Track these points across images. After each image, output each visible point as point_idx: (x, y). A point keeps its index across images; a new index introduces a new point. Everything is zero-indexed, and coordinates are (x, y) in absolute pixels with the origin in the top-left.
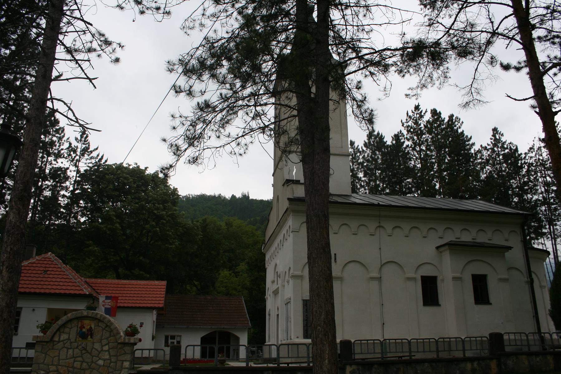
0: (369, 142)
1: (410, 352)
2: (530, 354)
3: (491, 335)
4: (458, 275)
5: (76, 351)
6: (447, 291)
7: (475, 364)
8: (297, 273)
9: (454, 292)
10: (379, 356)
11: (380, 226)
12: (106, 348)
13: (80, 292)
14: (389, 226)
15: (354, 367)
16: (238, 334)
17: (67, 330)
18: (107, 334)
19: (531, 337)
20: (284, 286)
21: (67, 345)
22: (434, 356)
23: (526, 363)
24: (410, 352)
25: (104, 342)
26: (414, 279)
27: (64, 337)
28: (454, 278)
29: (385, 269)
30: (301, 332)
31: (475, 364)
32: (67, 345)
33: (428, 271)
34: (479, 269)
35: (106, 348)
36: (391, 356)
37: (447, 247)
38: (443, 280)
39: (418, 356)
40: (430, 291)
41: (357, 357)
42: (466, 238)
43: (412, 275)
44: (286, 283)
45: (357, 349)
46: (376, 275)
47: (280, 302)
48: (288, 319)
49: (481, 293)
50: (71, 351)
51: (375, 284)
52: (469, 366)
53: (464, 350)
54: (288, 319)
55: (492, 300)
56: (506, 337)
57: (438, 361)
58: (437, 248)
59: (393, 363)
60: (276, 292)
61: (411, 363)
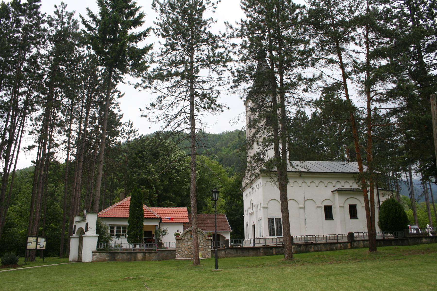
0: (297, 117)
1: (316, 240)
2: (364, 241)
3: (349, 233)
4: (342, 205)
5: (191, 243)
6: (336, 212)
7: (341, 245)
8: (265, 206)
9: (341, 213)
10: (304, 242)
11: (304, 182)
12: (202, 241)
13: (155, 217)
14: (308, 181)
15: (294, 246)
16: (225, 236)
17: (187, 235)
18: (202, 236)
19: (365, 234)
20: (257, 211)
21: (188, 240)
22: (325, 242)
23: (362, 244)
24: (316, 240)
25: (201, 239)
26: (321, 207)
27: (186, 238)
28: (340, 207)
29: (307, 202)
30: (268, 233)
31: (341, 245)
32: (188, 240)
33: (328, 203)
34: (352, 202)
35: (202, 241)
36: (309, 242)
37: (336, 192)
38: (335, 208)
39: (319, 242)
40: (328, 213)
41: (295, 242)
42: (347, 186)
43: (320, 205)
44: (258, 210)
45: (295, 240)
46: (303, 206)
47: (254, 218)
48: (260, 227)
49: (353, 214)
50: (189, 243)
51: (302, 209)
52: (339, 245)
53: (265, 243)
54: (260, 227)
55: (358, 217)
56: (355, 235)
57: (327, 243)
58: (332, 192)
59: (309, 244)
60: (252, 214)
61: (316, 244)
